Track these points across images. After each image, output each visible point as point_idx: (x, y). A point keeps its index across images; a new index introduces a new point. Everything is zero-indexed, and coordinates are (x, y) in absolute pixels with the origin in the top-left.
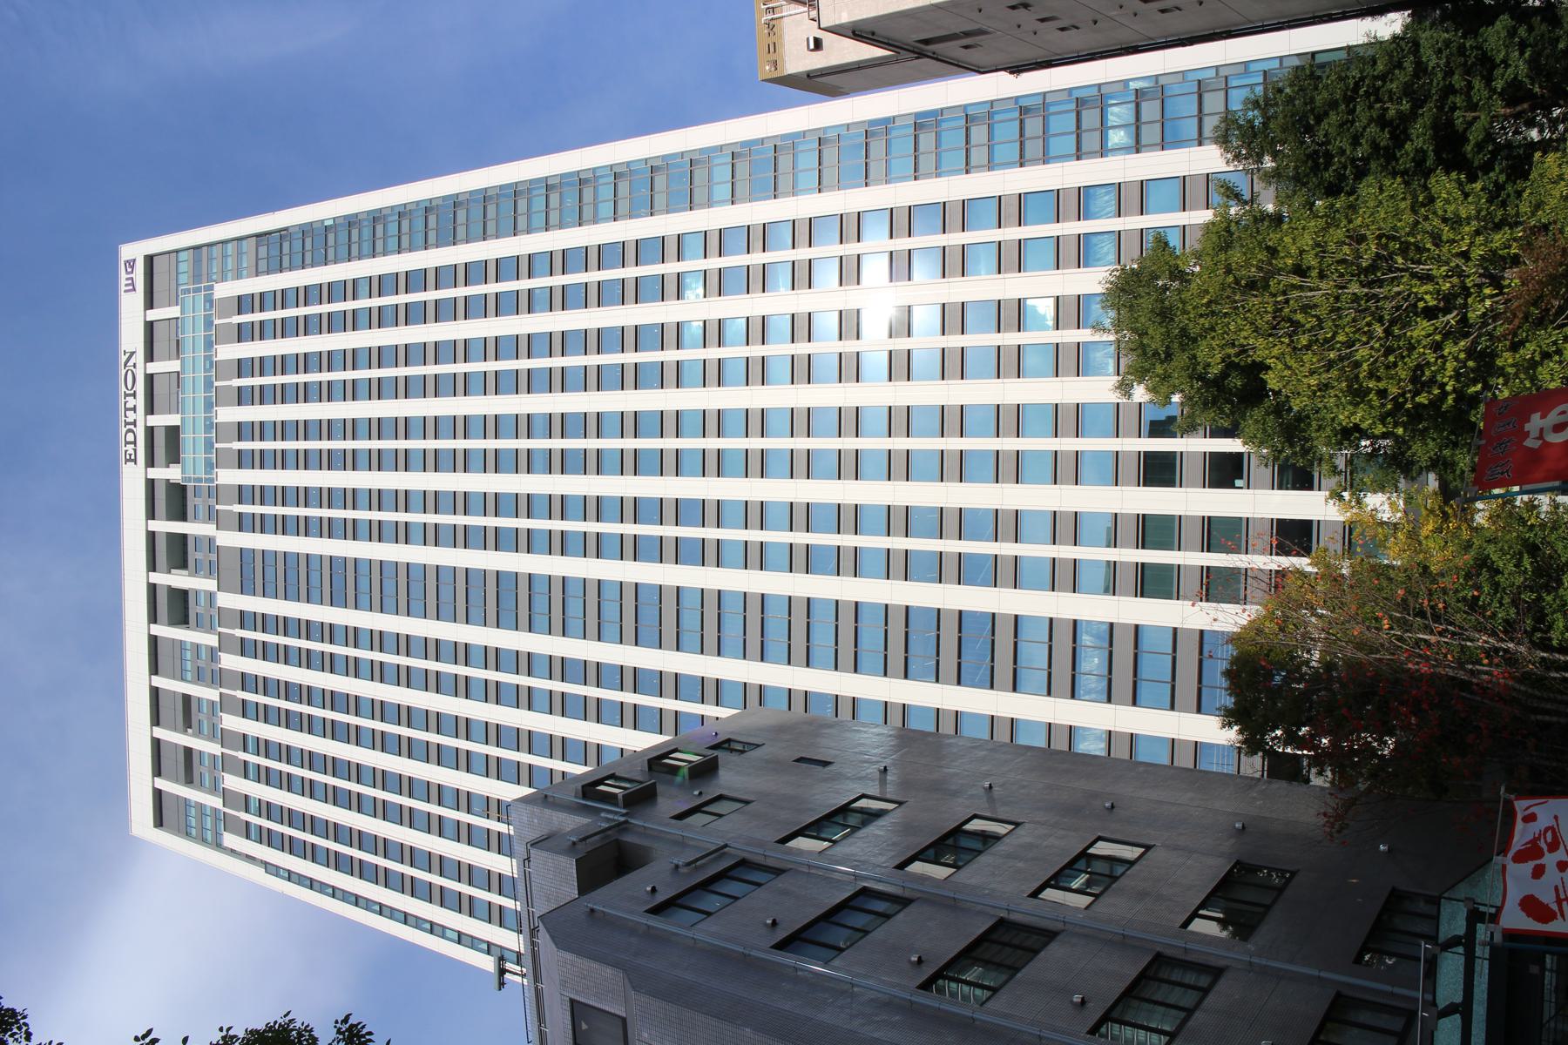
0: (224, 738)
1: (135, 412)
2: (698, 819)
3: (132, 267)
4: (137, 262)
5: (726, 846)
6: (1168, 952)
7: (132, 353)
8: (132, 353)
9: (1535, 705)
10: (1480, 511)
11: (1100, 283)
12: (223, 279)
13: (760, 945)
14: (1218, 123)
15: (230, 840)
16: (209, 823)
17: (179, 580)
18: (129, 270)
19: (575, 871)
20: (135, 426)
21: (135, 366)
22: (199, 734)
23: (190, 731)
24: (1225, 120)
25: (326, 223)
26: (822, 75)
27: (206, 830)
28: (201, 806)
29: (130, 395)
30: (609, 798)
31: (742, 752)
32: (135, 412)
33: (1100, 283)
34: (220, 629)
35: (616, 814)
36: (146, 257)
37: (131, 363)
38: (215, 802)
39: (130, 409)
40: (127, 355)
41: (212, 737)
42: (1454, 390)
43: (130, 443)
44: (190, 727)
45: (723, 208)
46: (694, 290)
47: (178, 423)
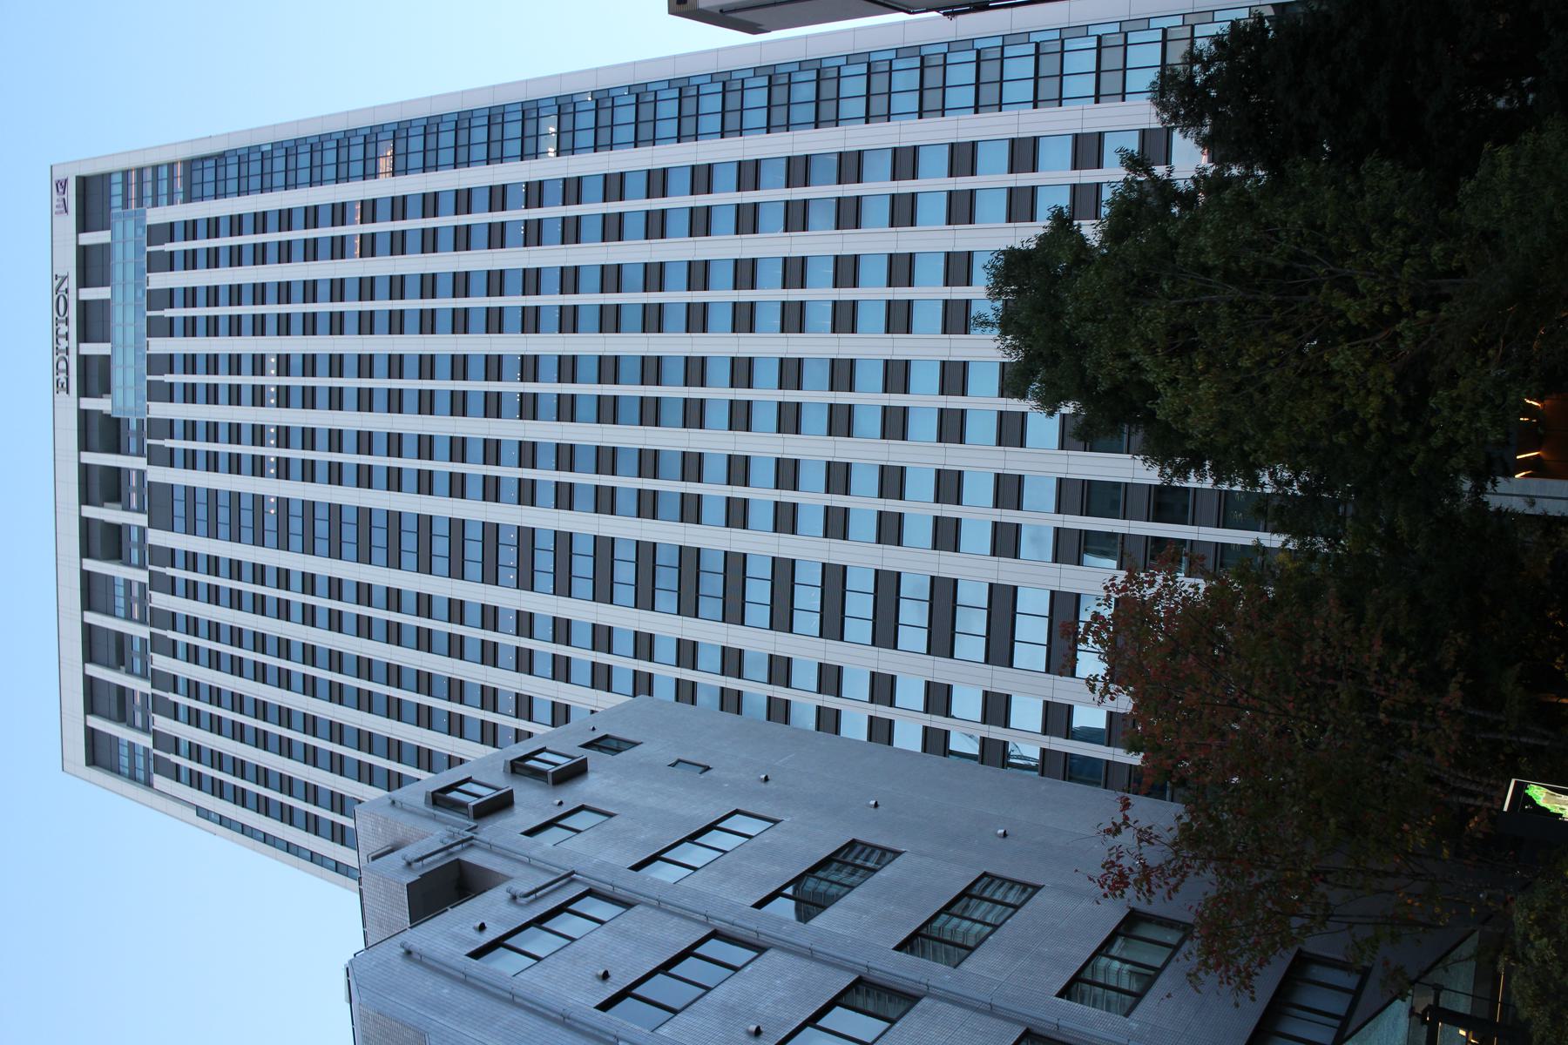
0: (157, 678)
1: (67, 339)
2: (554, 833)
3: (64, 188)
4: (69, 181)
5: (573, 872)
6: (1036, 1030)
7: (65, 278)
8: (65, 278)
9: (1458, 785)
10: (1293, 806)
11: (985, 267)
12: (155, 204)
13: (583, 998)
14: (1155, 79)
15: (159, 781)
16: (140, 762)
17: (110, 514)
18: (61, 190)
19: (406, 897)
20: (67, 354)
21: (67, 291)
22: (130, 672)
23: (123, 668)
24: (1162, 75)
25: (265, 149)
26: (735, 10)
27: (140, 769)
28: (132, 745)
29: (62, 322)
30: (457, 806)
31: (618, 751)
32: (67, 339)
33: (985, 267)
34: (151, 568)
35: (462, 822)
36: (78, 178)
37: (63, 288)
38: (146, 741)
39: (62, 336)
40: (59, 280)
41: (143, 676)
42: (1379, 428)
43: (62, 371)
44: (123, 664)
45: (668, 146)
46: (821, 217)
47: (108, 352)
